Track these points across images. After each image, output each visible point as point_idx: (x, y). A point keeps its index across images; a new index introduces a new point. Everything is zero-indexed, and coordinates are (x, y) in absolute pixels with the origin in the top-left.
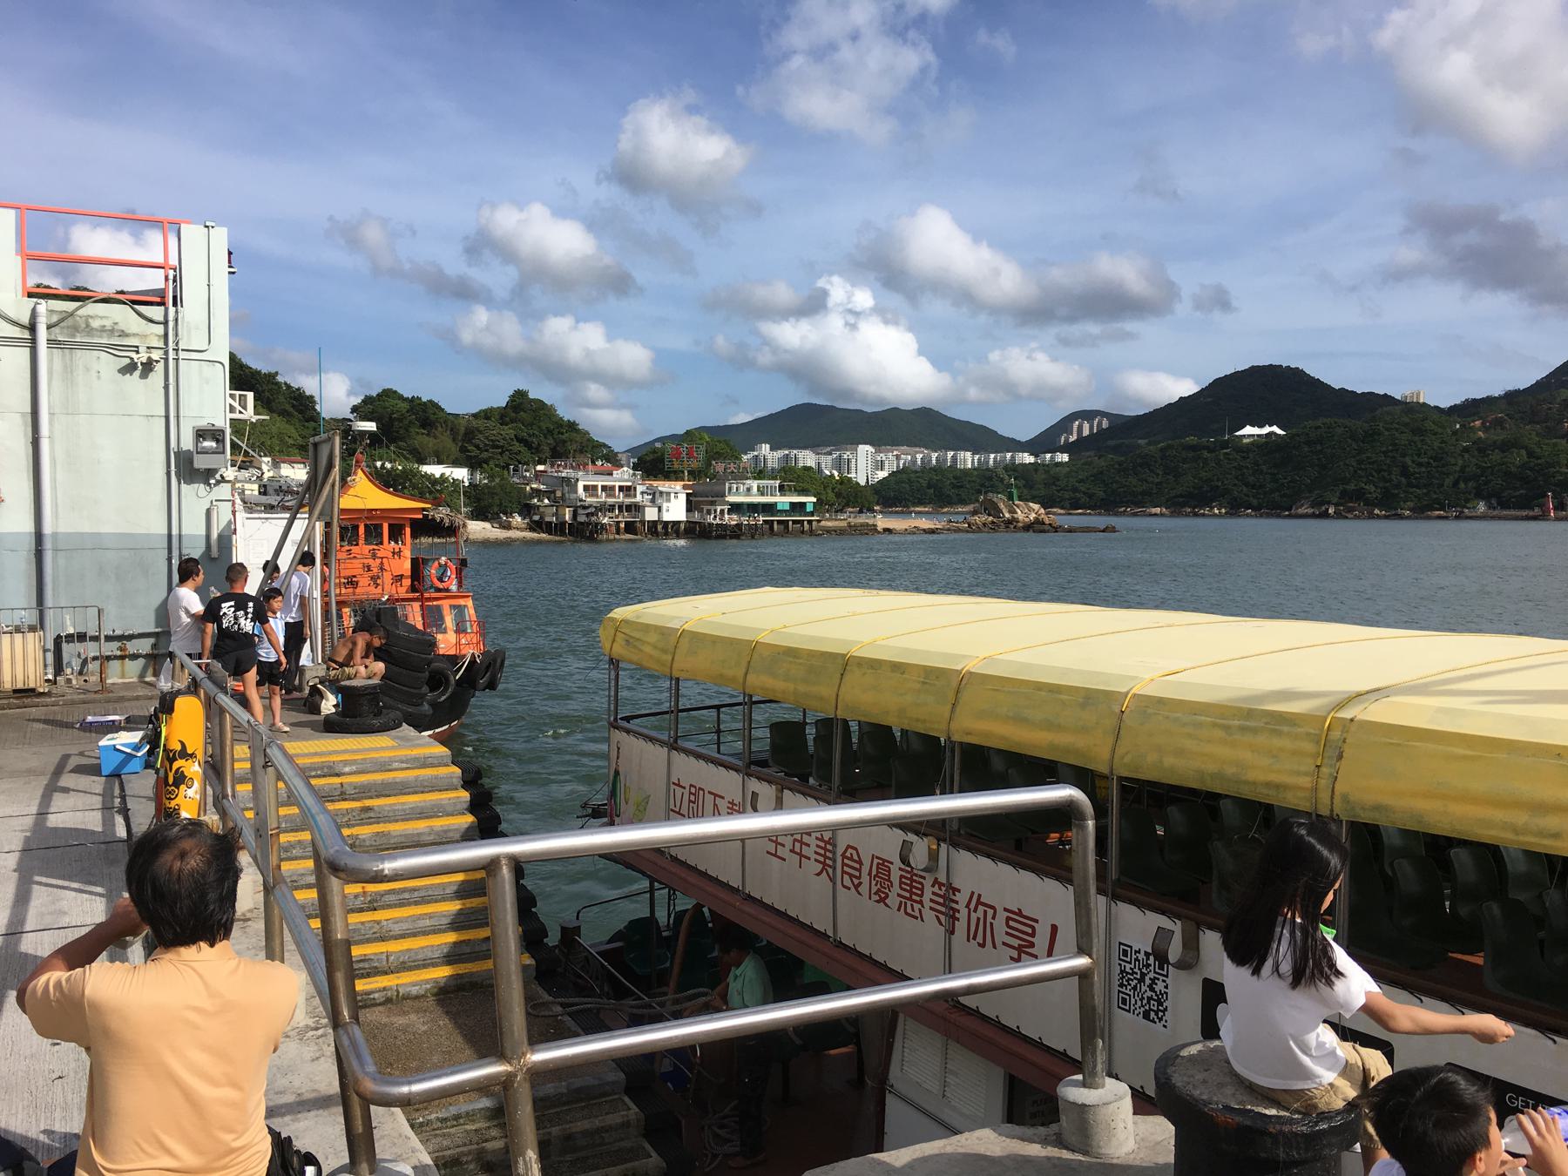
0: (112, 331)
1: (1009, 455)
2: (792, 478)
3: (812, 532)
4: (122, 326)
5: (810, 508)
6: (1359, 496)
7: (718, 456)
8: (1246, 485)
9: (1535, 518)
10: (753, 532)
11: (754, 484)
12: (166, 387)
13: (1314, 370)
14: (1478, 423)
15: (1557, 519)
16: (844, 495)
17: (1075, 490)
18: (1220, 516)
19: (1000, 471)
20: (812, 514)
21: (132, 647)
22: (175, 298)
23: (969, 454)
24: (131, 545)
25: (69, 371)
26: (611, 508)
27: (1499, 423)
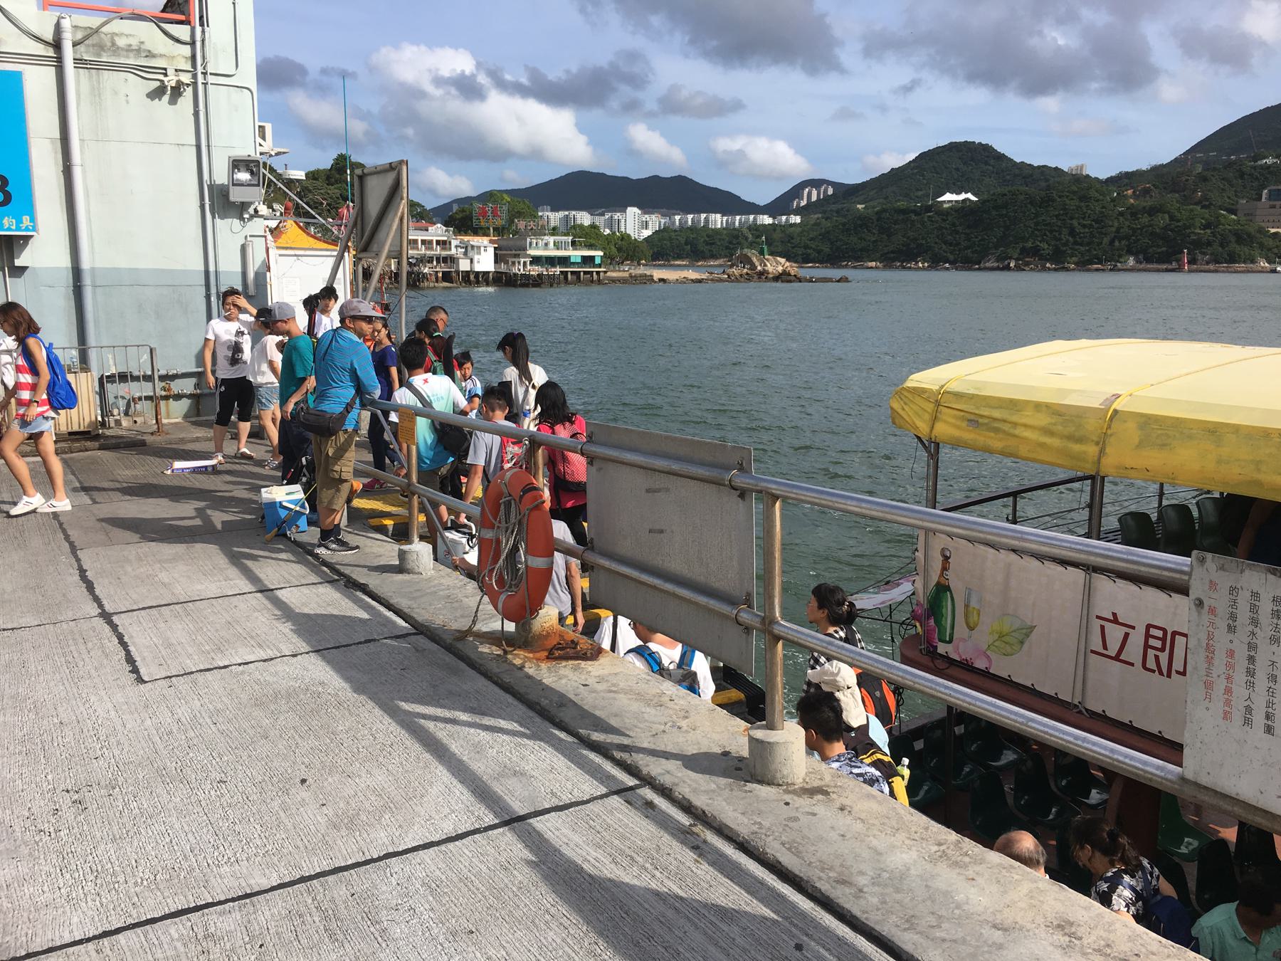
0: (138, 51)
1: (751, 217)
2: (585, 237)
3: (599, 282)
4: (148, 46)
5: (598, 261)
6: (1035, 252)
7: (520, 214)
8: (945, 243)
9: (1173, 270)
10: (552, 281)
11: (551, 240)
12: (196, 114)
13: (1000, 147)
14: (1130, 192)
15: (1190, 271)
16: (624, 250)
17: (806, 247)
18: (924, 269)
19: (745, 231)
20: (600, 266)
21: (177, 387)
22: (201, 18)
23: (719, 216)
24: (169, 281)
25: (96, 93)
26: (430, 260)
27: (1146, 192)
